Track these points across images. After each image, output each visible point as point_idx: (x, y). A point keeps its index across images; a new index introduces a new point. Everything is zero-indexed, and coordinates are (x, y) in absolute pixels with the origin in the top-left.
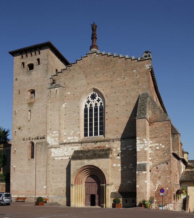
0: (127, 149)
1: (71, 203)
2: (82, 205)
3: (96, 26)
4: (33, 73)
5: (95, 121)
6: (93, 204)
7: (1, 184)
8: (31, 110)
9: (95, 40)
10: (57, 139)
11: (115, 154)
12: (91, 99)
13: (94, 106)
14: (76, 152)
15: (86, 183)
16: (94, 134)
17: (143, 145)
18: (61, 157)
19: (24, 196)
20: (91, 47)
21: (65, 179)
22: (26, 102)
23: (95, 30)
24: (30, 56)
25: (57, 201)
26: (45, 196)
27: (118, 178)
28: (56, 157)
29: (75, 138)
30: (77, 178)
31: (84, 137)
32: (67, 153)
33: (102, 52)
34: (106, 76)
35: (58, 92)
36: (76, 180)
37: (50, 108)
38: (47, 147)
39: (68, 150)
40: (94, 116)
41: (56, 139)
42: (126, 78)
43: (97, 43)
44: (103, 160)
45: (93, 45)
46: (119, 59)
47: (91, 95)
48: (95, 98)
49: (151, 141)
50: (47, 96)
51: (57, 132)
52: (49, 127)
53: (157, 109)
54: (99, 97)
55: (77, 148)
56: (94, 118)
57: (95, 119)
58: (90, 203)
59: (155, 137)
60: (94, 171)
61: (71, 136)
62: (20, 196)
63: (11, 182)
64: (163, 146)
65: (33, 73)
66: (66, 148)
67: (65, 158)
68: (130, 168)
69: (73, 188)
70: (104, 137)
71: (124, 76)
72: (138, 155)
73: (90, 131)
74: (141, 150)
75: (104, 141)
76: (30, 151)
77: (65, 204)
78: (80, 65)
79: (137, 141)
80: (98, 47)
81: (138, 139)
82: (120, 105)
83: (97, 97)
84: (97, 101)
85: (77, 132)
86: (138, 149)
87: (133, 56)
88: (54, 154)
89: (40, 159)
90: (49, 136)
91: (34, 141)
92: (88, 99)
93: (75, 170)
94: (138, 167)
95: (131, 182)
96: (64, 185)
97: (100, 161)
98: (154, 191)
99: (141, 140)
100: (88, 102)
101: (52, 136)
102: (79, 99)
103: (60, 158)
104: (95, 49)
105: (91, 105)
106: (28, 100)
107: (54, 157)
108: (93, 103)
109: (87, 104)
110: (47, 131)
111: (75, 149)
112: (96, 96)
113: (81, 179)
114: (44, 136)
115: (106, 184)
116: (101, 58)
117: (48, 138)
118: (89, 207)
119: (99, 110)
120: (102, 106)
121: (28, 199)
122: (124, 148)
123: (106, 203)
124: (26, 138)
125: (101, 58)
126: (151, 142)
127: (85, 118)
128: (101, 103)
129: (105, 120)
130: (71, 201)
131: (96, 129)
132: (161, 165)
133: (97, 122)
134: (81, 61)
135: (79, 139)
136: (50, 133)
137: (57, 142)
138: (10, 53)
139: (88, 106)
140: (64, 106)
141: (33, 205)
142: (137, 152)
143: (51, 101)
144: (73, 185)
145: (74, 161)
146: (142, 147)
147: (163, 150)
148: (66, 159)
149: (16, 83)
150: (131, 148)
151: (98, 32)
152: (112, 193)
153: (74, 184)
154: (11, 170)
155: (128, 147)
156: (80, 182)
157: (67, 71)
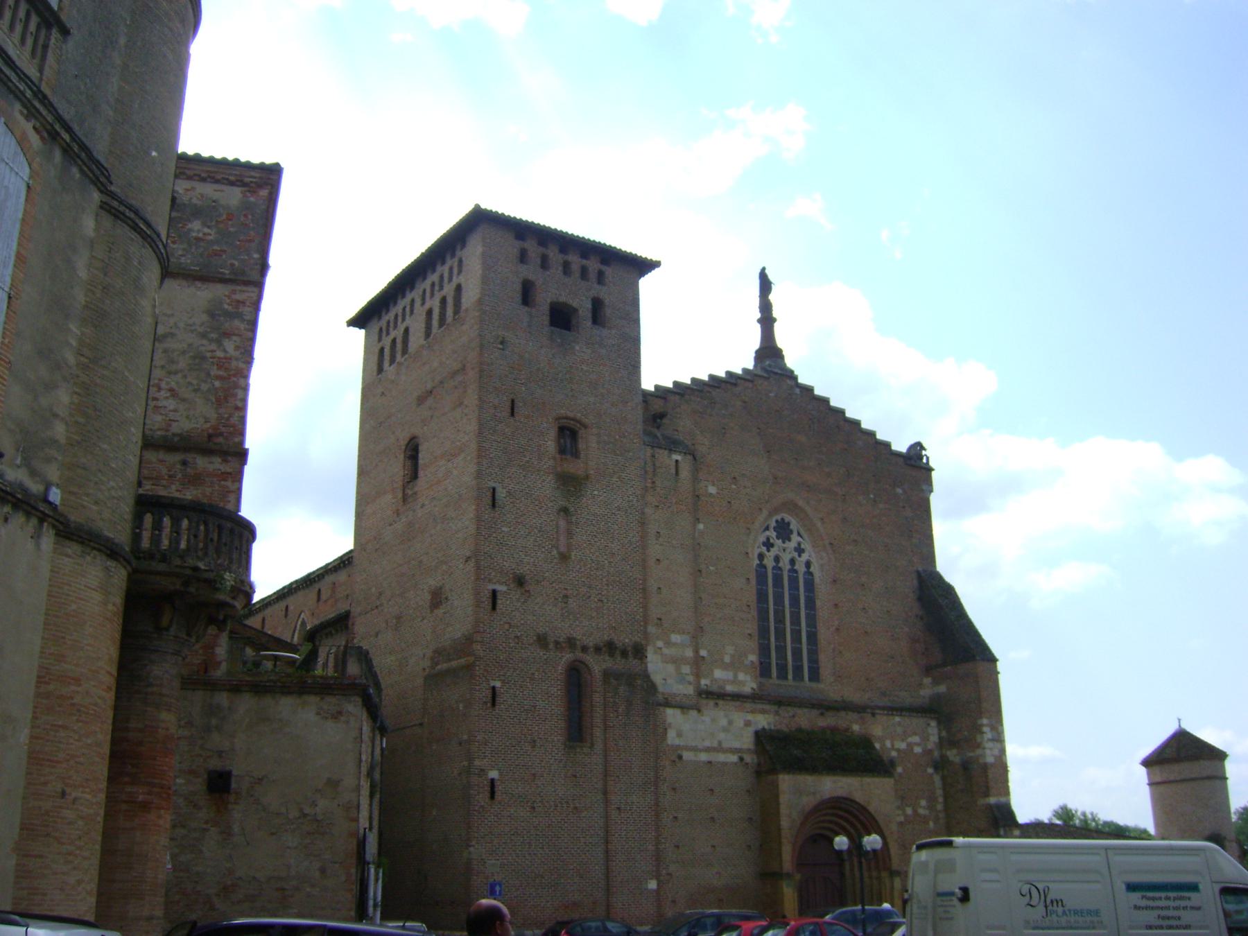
0: (910, 745)
18: (708, 750)
39: (730, 723)
60: (846, 815)
61: (725, 667)
65: (577, 348)
66: (726, 716)
67: (721, 757)
81: (987, 725)
83: (795, 538)
88: (679, 735)
91: (590, 659)
100: (768, 545)
101: (666, 651)
103: (704, 757)
105: (777, 559)
107: (678, 747)
136: (658, 638)
138: (764, 269)
148: (725, 764)
155: (910, 740)
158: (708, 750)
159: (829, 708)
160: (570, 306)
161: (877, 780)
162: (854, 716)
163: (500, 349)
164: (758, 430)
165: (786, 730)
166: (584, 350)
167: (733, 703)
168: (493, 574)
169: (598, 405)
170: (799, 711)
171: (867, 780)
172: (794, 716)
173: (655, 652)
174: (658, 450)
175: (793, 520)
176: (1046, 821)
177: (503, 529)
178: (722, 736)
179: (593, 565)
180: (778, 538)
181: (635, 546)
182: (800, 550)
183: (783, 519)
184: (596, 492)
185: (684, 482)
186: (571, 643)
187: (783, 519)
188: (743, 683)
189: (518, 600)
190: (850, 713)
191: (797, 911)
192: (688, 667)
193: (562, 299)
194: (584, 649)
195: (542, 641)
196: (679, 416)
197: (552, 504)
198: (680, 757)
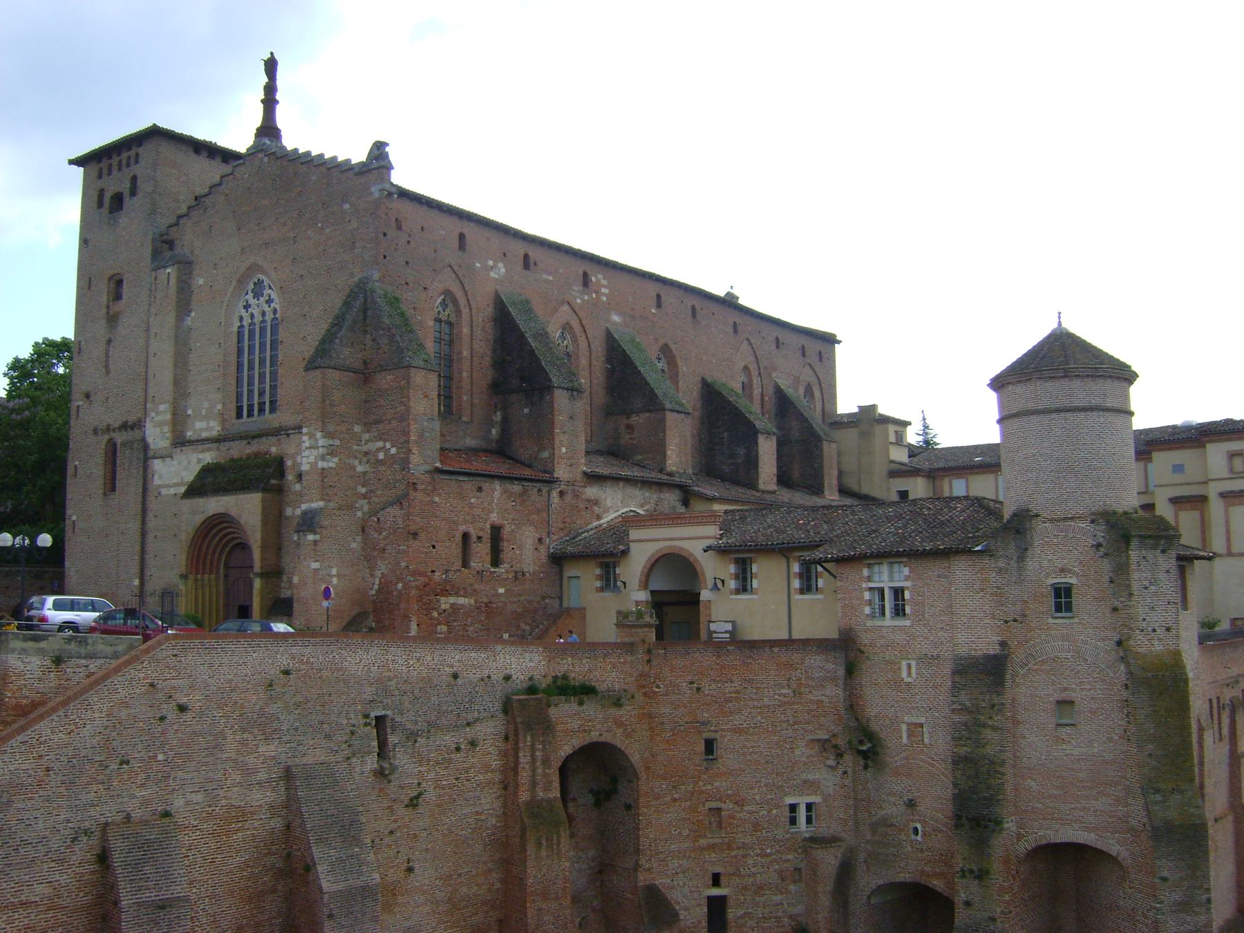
13: (258, 319)
14: (206, 471)
38: (146, 454)
49: (368, 434)
55: (209, 457)
76: (1232, 536)
78: (227, 191)
82: (311, 317)
99: (312, 436)
126: (366, 436)
159: (254, 437)
161: (248, 496)
165: (223, 461)
167: (191, 447)
170: (232, 444)
171: (242, 497)
172: (229, 449)
176: (1208, 446)
182: (269, 301)
190: (270, 438)
192: (167, 427)
198: (160, 494)
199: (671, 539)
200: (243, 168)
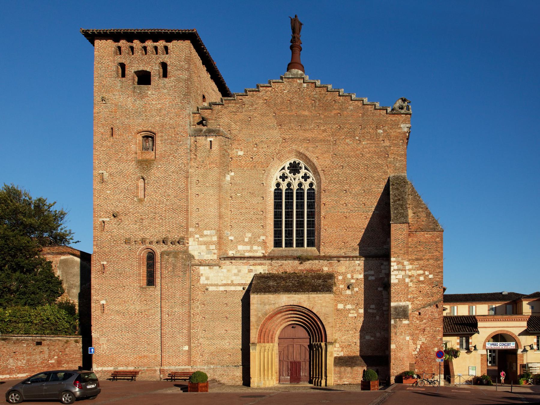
1: (252, 381)
2: (274, 382)
3: (301, 24)
4: (149, 93)
5: (297, 218)
6: (295, 378)
7: (59, 340)
8: (145, 177)
9: (298, 51)
10: (213, 247)
11: (342, 286)
12: (290, 173)
13: (295, 187)
14: (259, 277)
15: (279, 339)
16: (296, 244)
17: (403, 273)
18: (225, 285)
19: (131, 368)
20: (290, 67)
21: (239, 333)
22: (131, 156)
23: (297, 30)
24: (142, 53)
25: (216, 377)
26: (187, 367)
27: (348, 331)
28: (212, 285)
29: (255, 248)
30: (264, 330)
31: (273, 248)
32: (239, 278)
33: (316, 81)
34: (325, 131)
35: (215, 147)
36: (262, 334)
37: (194, 179)
40: (297, 208)
41: (211, 248)
42: (363, 143)
43: (303, 57)
44: (320, 295)
45: (293, 62)
46: (351, 102)
47: (290, 164)
48: (299, 173)
50: (189, 151)
51: (213, 232)
52: (194, 220)
53: (422, 208)
54: (306, 171)
55: (261, 269)
56: (297, 212)
57: (297, 215)
58: (289, 377)
59: (417, 259)
61: (246, 244)
62: (121, 369)
63: (93, 337)
64: (431, 276)
65: (149, 93)
66: (236, 268)
67: (233, 288)
68: (370, 313)
69: (255, 349)
70: (319, 252)
71: (360, 138)
72: (393, 290)
73: (286, 237)
74: (399, 281)
75: (318, 258)
77: (240, 382)
78: (267, 98)
79: (392, 264)
80: (303, 67)
81: (394, 262)
82: (351, 193)
83: (303, 172)
84: (302, 177)
85: (259, 237)
86: (394, 280)
87: (365, 97)
88: (207, 279)
89: (172, 288)
90: (194, 240)
91: (154, 247)
92: (283, 171)
93: (260, 315)
94: (392, 311)
95: (372, 339)
96: (238, 343)
97: (314, 298)
98: (414, 353)
99: (398, 263)
100: (284, 177)
101: (201, 239)
102: (265, 167)
103: (222, 289)
104: (300, 72)
105: (289, 185)
106: (136, 153)
107: (207, 285)
108: (295, 180)
109: (280, 181)
110: (187, 228)
111: (256, 270)
112: (301, 168)
113: (271, 333)
114: (183, 238)
115: (326, 341)
116: (314, 93)
117: (190, 244)
118: (288, 385)
119: (307, 197)
120: (314, 189)
121: (141, 374)
122: (359, 275)
123: (326, 376)
124: (133, 239)
125: (314, 93)
126: (410, 267)
127: (275, 209)
128: (311, 184)
129: (319, 218)
130: (251, 376)
131: (300, 234)
132: (427, 308)
133: (303, 221)
134: (270, 89)
135: (264, 252)
136: (196, 234)
137: (215, 254)
139: (284, 187)
140: (228, 178)
141: (359, 390)
142: (392, 285)
143: (198, 163)
144: (256, 344)
145: (259, 296)
146: (400, 277)
147: (431, 282)
149: (100, 110)
150: (373, 275)
151: (304, 36)
152: (335, 358)
153: (258, 342)
154: (92, 310)
156: (270, 337)
157: (236, 104)
158: (225, 285)
160: (146, 71)
162: (326, 262)
163: (104, 103)
164: (274, 114)
166: (154, 93)
168: (102, 213)
169: (162, 120)
173: (194, 240)
174: (198, 137)
175: (301, 162)
177: (107, 192)
178: (234, 278)
179: (157, 202)
180: (290, 173)
181: (182, 189)
183: (299, 164)
184: (159, 166)
185: (215, 152)
186: (143, 241)
187: (299, 164)
188: (256, 251)
189: (115, 224)
191: (492, 336)
193: (141, 69)
194: (151, 243)
195: (127, 241)
196: (221, 116)
197: (134, 176)
198: (207, 289)
199: (499, 327)
200: (281, 86)
